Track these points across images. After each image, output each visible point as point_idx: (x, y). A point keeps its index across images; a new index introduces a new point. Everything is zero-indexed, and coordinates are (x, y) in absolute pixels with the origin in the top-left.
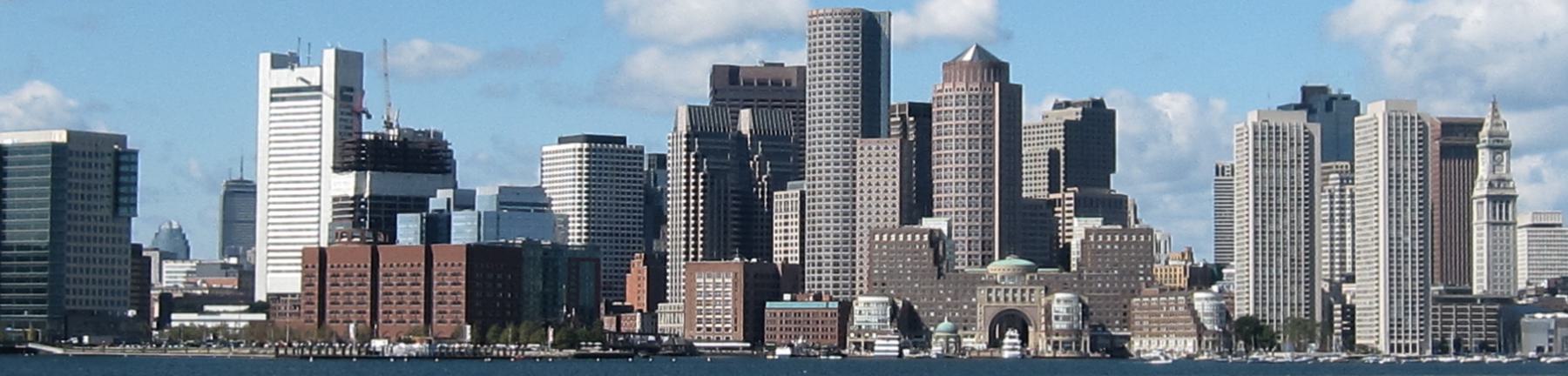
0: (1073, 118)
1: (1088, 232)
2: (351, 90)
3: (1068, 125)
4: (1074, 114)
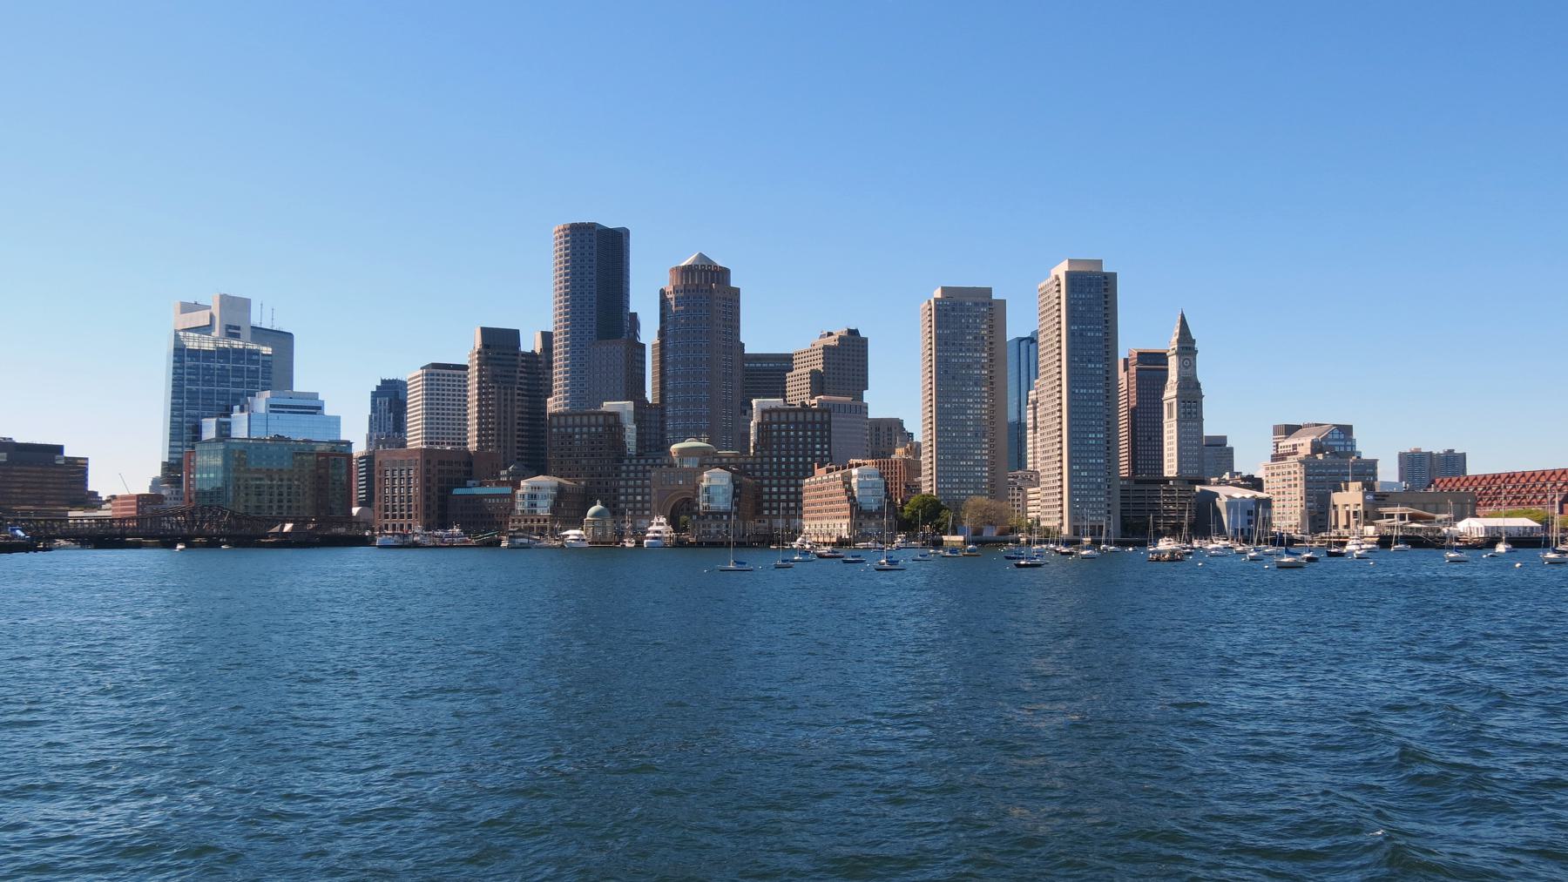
0: (832, 344)
1: (764, 412)
2: (238, 328)
3: (826, 348)
4: (832, 341)
